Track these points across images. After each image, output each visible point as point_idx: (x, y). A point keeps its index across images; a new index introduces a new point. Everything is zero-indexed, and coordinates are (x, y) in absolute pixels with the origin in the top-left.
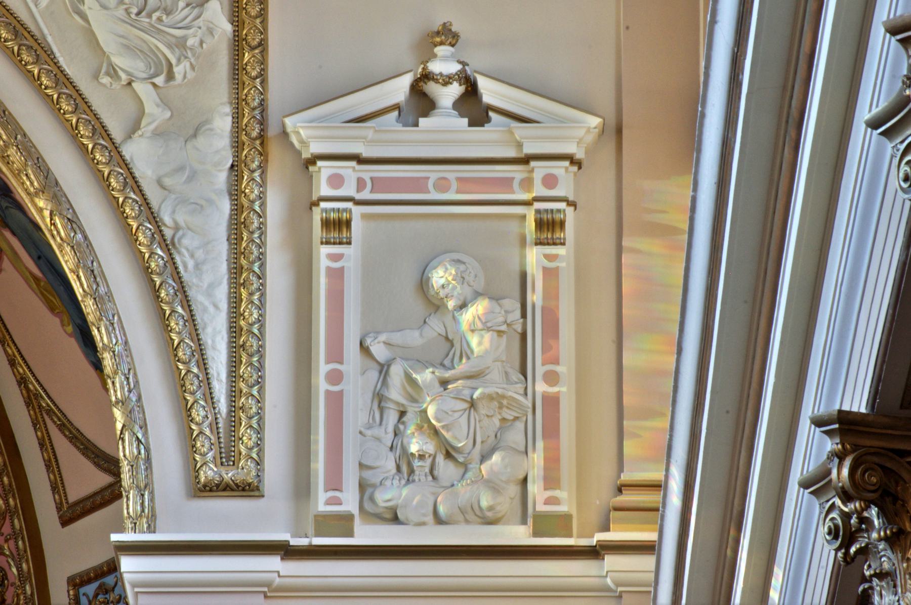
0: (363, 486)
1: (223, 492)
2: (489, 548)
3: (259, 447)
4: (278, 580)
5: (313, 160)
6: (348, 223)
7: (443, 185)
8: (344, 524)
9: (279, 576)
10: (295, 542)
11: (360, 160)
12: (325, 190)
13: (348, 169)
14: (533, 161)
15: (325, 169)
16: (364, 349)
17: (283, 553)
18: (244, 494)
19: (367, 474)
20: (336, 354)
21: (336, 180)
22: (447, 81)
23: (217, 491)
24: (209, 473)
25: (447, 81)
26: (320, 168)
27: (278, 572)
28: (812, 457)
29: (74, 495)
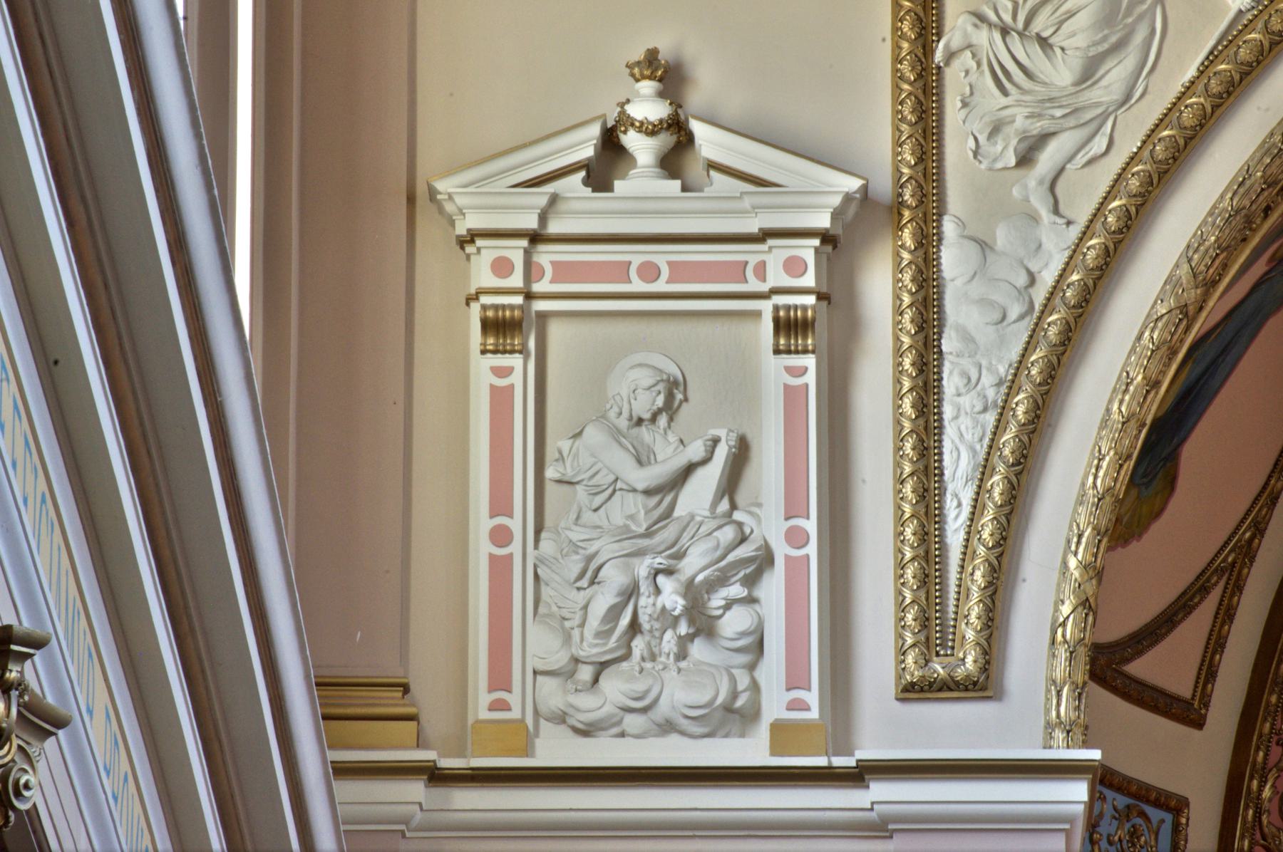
1: (940, 693)
2: (637, 771)
3: (990, 629)
4: (419, 816)
7: (649, 272)
9: (422, 809)
10: (446, 763)
14: (771, 239)
17: (425, 777)
18: (922, 695)
23: (930, 691)
26: (479, 249)
27: (420, 804)
28: (57, 647)
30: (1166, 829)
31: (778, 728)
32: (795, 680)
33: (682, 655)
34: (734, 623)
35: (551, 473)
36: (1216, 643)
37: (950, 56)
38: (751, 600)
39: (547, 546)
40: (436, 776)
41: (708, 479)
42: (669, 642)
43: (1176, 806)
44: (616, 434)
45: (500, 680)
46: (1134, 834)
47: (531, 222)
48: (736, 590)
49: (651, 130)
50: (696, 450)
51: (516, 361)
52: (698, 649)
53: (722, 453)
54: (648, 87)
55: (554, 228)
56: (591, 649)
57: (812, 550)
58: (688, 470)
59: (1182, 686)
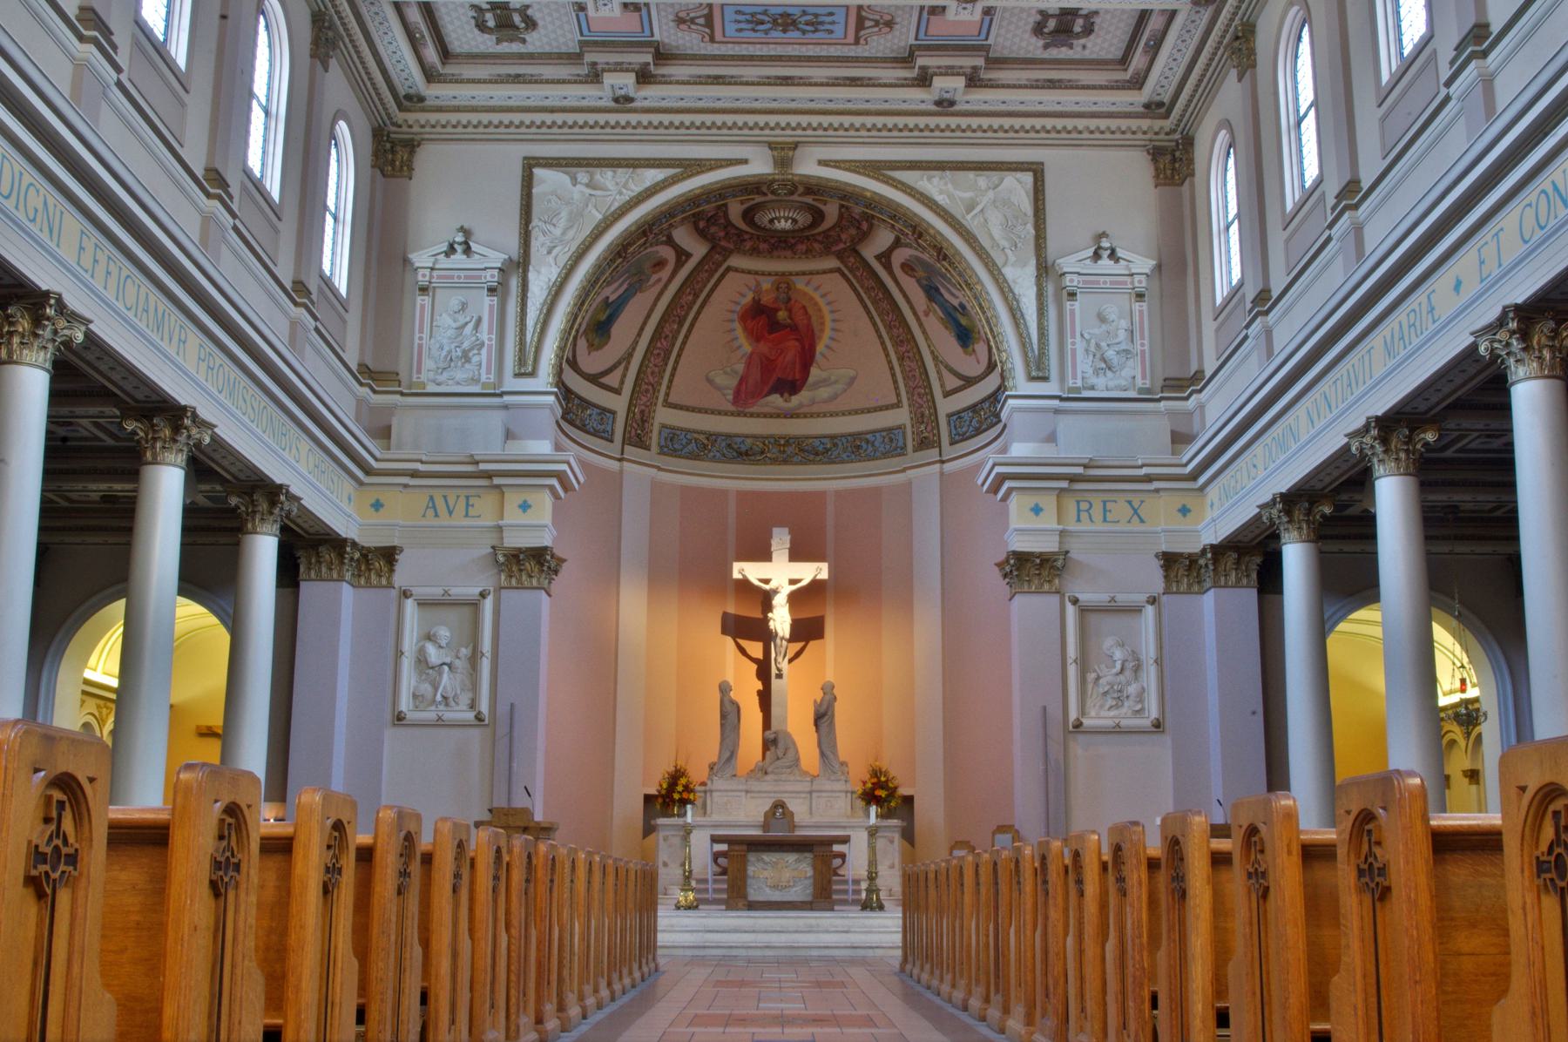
0: (1083, 378)
5: (1064, 274)
6: (1076, 294)
7: (1105, 283)
8: (1078, 390)
10: (405, 391)
11: (1079, 274)
12: (1068, 284)
13: (1075, 277)
15: (1068, 277)
16: (1082, 335)
19: (1085, 375)
20: (1073, 336)
21: (1140, 282)
22: (1106, 249)
24: (1034, 374)
25: (1106, 249)
29: (948, 388)
30: (611, 419)
31: (483, 383)
32: (489, 372)
33: (463, 366)
34: (475, 359)
35: (435, 324)
36: (624, 376)
37: (533, 228)
38: (479, 354)
39: (433, 341)
40: (402, 394)
41: (470, 326)
42: (460, 364)
43: (613, 413)
44: (449, 315)
45: (419, 371)
46: (602, 419)
47: (431, 265)
48: (475, 352)
49: (460, 244)
50: (468, 319)
51: (426, 298)
52: (467, 366)
53: (474, 320)
54: (461, 234)
55: (437, 266)
56: (442, 365)
57: (494, 342)
58: (467, 323)
59: (616, 385)
